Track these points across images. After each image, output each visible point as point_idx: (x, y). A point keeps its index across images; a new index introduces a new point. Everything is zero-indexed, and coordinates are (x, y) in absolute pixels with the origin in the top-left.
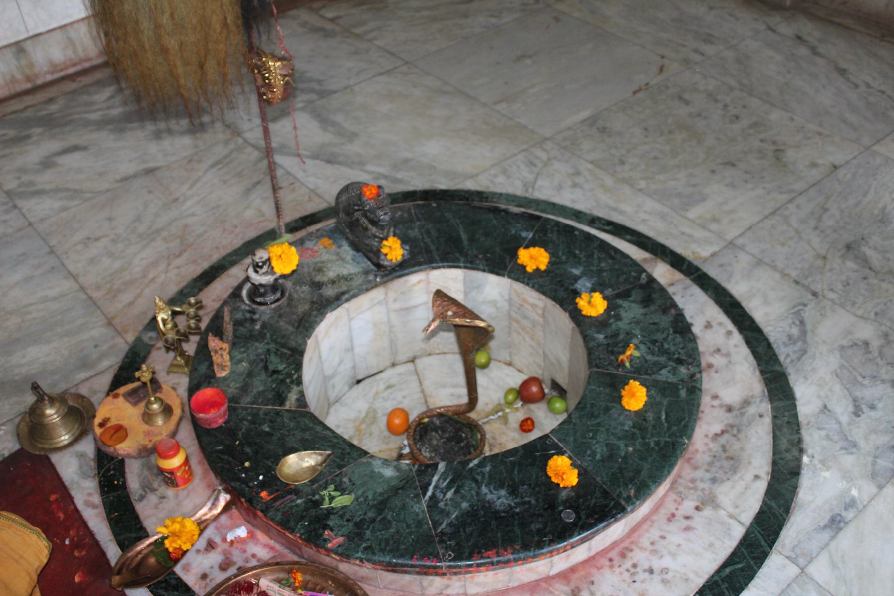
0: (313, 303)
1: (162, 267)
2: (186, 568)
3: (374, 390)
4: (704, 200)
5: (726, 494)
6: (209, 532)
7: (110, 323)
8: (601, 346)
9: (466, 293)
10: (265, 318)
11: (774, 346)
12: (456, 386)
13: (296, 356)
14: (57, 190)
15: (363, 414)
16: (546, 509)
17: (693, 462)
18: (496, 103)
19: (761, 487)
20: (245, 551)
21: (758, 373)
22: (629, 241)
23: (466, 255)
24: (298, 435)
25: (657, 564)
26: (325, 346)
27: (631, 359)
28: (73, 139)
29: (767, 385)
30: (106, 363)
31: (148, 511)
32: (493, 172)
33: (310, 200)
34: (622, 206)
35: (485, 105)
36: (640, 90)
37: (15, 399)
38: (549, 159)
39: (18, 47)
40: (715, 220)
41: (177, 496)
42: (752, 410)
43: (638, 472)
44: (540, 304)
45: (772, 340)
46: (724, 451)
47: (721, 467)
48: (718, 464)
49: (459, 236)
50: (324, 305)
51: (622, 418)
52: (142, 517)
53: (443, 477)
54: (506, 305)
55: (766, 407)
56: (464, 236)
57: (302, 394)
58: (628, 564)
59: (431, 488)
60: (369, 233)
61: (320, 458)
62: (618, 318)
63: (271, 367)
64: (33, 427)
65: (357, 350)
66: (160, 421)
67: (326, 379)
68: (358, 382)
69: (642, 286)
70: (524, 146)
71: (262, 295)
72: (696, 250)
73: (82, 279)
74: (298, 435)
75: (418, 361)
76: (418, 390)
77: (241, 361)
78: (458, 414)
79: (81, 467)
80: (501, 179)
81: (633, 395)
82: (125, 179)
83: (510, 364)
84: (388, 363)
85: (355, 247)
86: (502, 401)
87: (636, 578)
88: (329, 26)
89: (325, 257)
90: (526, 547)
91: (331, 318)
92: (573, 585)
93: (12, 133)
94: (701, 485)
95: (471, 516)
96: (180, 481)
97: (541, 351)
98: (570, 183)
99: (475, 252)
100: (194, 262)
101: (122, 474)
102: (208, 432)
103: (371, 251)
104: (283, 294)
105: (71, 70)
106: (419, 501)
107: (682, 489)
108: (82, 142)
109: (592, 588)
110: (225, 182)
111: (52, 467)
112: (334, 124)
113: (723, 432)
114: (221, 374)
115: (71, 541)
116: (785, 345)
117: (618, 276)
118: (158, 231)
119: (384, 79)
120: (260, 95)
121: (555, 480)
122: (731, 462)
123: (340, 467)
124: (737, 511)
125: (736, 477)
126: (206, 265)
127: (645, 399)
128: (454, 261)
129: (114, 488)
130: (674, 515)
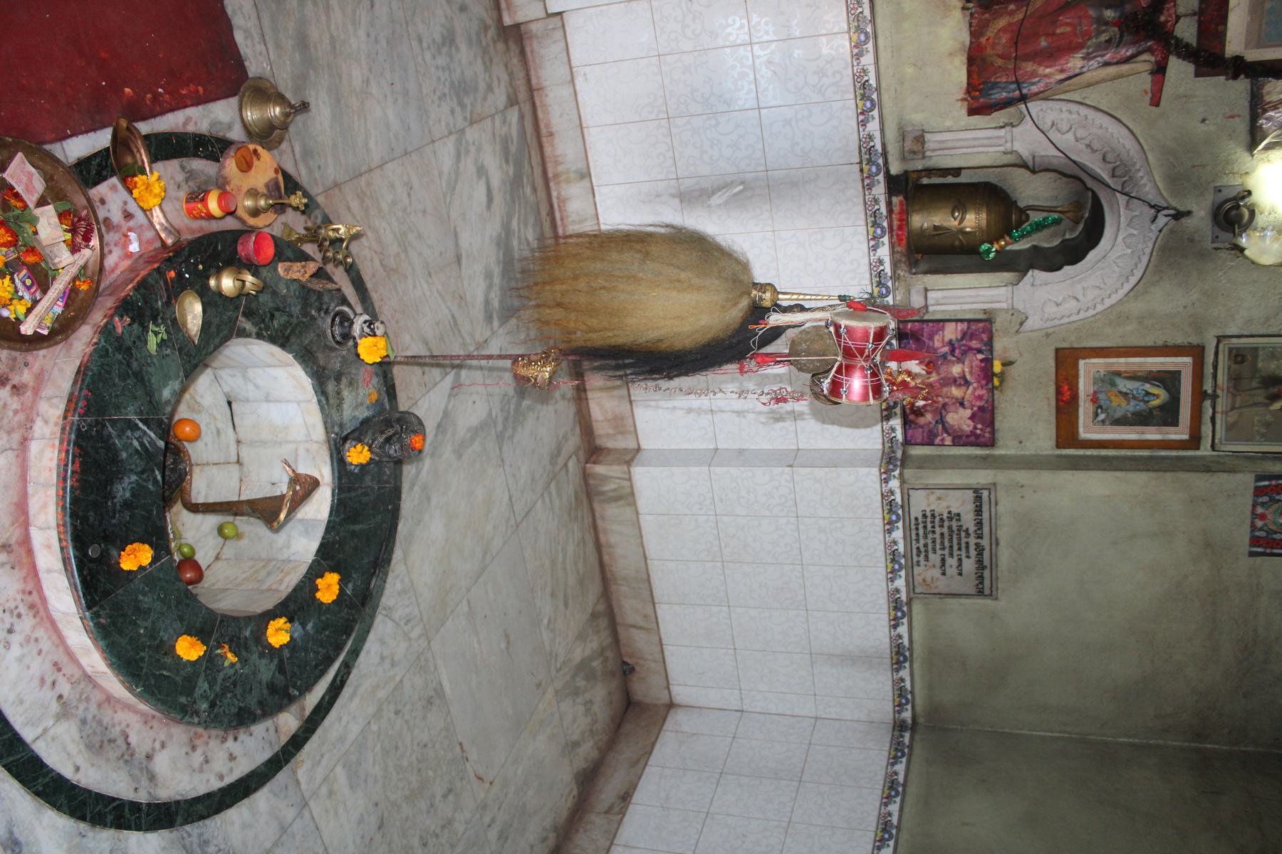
0: (324, 369)
1: (374, 245)
2: (113, 188)
3: (218, 416)
4: (351, 787)
5: (68, 731)
6: (140, 216)
7: (336, 185)
8: (236, 631)
9: (301, 521)
10: (319, 322)
11: (201, 823)
12: (206, 496)
13: (281, 340)
14: (457, 173)
15: (198, 399)
16: (104, 531)
17: (106, 705)
18: (469, 602)
19: (67, 772)
20: (116, 245)
21: (179, 798)
22: (323, 698)
23: (340, 524)
24: (216, 321)
25: (16, 639)
26: (280, 373)
27: (224, 657)
28: (498, 199)
29: (164, 804)
30: (303, 172)
31: (171, 168)
32: (406, 580)
33: (409, 398)
34: (357, 700)
35: (469, 590)
36: (463, 750)
37: (290, 84)
38: (410, 639)
39: (585, 175)
40: (331, 793)
41: (177, 199)
42: (144, 782)
43: (120, 632)
44: (282, 587)
45: (207, 822)
46: (110, 741)
47: (94, 733)
48: (99, 730)
49: (359, 523)
50: (320, 378)
51: (171, 631)
52: (167, 162)
53: (152, 443)
54: (285, 556)
55: (142, 798)
56: (357, 527)
57: (249, 336)
58: (22, 609)
59: (145, 428)
60: (378, 435)
61: (193, 333)
62: (262, 655)
63: (277, 314)
64: (264, 93)
65: (265, 405)
66: (249, 203)
67: (244, 369)
68: (230, 403)
69: (286, 687)
70: (425, 618)
71: (341, 323)
72: (306, 764)
73: (378, 172)
74: (216, 321)
75: (237, 466)
76: (210, 460)
77: (288, 288)
78: (182, 491)
79: (220, 123)
80: (399, 586)
81: (192, 646)
82: (456, 236)
83: (217, 558)
84: (242, 436)
85: (365, 422)
86: (183, 541)
87: (7, 614)
88: (561, 460)
89: (361, 392)
90: (74, 501)
91: (307, 382)
92: (15, 547)
93: (513, 149)
94: (82, 707)
95: (114, 459)
96: (191, 205)
97: (229, 586)
98: (385, 654)
99: (342, 534)
100: (374, 276)
101: (207, 157)
102: (235, 242)
103: (361, 434)
104: (338, 343)
105: (558, 215)
106: (136, 413)
107: (82, 685)
108: (495, 206)
109: (8, 567)
110: (437, 324)
111: (226, 96)
112: (473, 439)
113: (128, 744)
114: (281, 268)
115: (160, 94)
116: (201, 835)
117: (299, 667)
118: (406, 251)
119: (506, 499)
120: (522, 356)
121: (129, 548)
122: (97, 745)
123: (180, 350)
124: (49, 739)
125: (82, 747)
126: (369, 285)
127: (185, 658)
128: (337, 511)
129: (196, 146)
130: (59, 670)
